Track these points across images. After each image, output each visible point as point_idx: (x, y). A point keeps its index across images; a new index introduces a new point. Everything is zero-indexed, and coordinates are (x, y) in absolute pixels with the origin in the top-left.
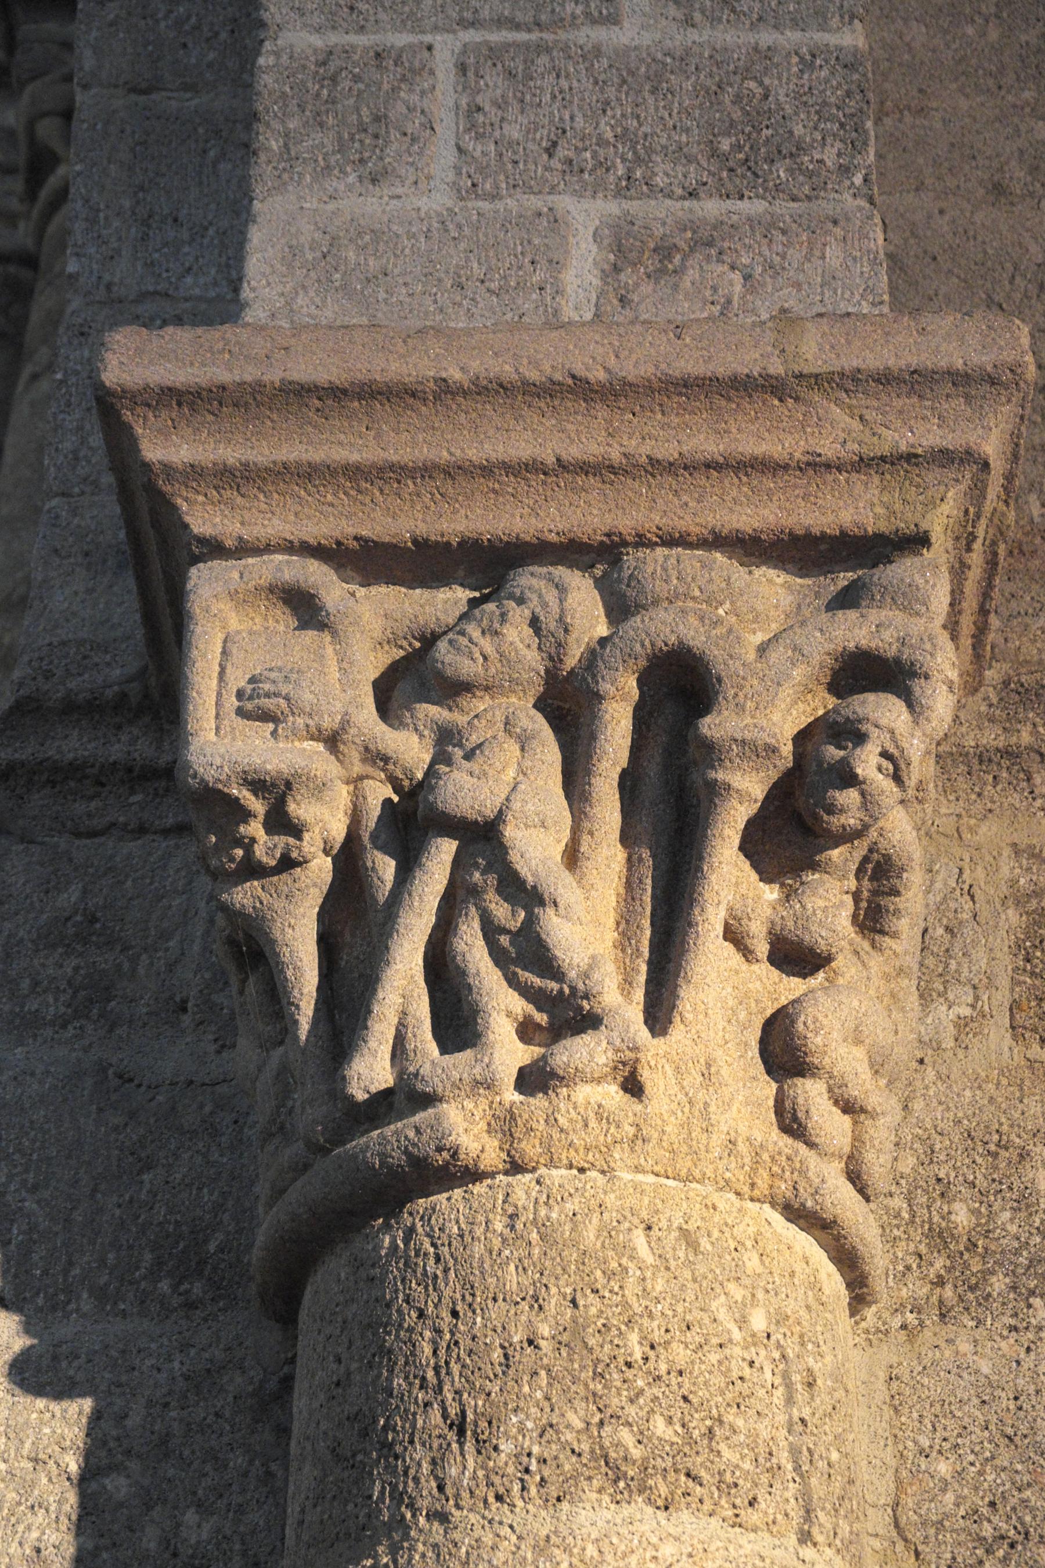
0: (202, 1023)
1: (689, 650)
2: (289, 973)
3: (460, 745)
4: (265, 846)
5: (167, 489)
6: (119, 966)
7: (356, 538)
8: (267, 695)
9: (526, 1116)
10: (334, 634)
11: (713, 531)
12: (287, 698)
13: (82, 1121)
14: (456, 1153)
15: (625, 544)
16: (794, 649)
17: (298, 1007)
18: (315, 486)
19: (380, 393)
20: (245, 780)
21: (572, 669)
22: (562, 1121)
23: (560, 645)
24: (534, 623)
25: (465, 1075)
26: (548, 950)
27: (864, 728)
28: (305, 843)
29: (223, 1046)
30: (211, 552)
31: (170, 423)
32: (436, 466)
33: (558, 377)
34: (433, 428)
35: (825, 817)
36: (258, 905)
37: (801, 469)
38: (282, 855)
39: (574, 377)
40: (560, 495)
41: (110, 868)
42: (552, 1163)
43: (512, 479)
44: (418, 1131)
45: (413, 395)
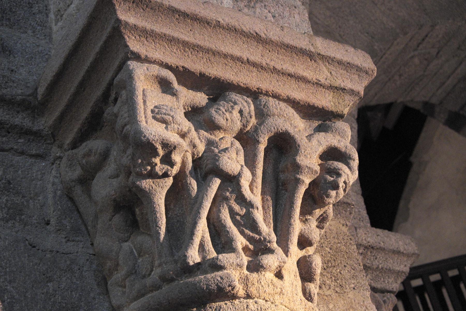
0: (59, 230)
1: (289, 134)
2: (158, 215)
3: (217, 147)
4: (160, 168)
5: (123, 31)
6: (23, 203)
7: (183, 67)
8: (165, 114)
9: (252, 279)
10: (177, 98)
11: (288, 96)
12: (173, 117)
13: (23, 259)
14: (234, 288)
15: (261, 93)
16: (318, 142)
17: (160, 228)
18: (171, 45)
19: (198, 20)
20: (162, 142)
21: (248, 131)
22: (262, 283)
23: (248, 121)
24: (241, 112)
25: (234, 262)
26: (257, 224)
27: (341, 172)
28: (173, 170)
29: (68, 240)
30: (135, 58)
31: (128, 8)
32: (211, 50)
33: (252, 32)
34: (211, 37)
35: (326, 198)
36: (151, 188)
37: (313, 84)
38: (165, 172)
39: (256, 33)
40: (244, 71)
41: (12, 165)
42: (259, 297)
43: (232, 61)
44: (222, 278)
45: (208, 24)
